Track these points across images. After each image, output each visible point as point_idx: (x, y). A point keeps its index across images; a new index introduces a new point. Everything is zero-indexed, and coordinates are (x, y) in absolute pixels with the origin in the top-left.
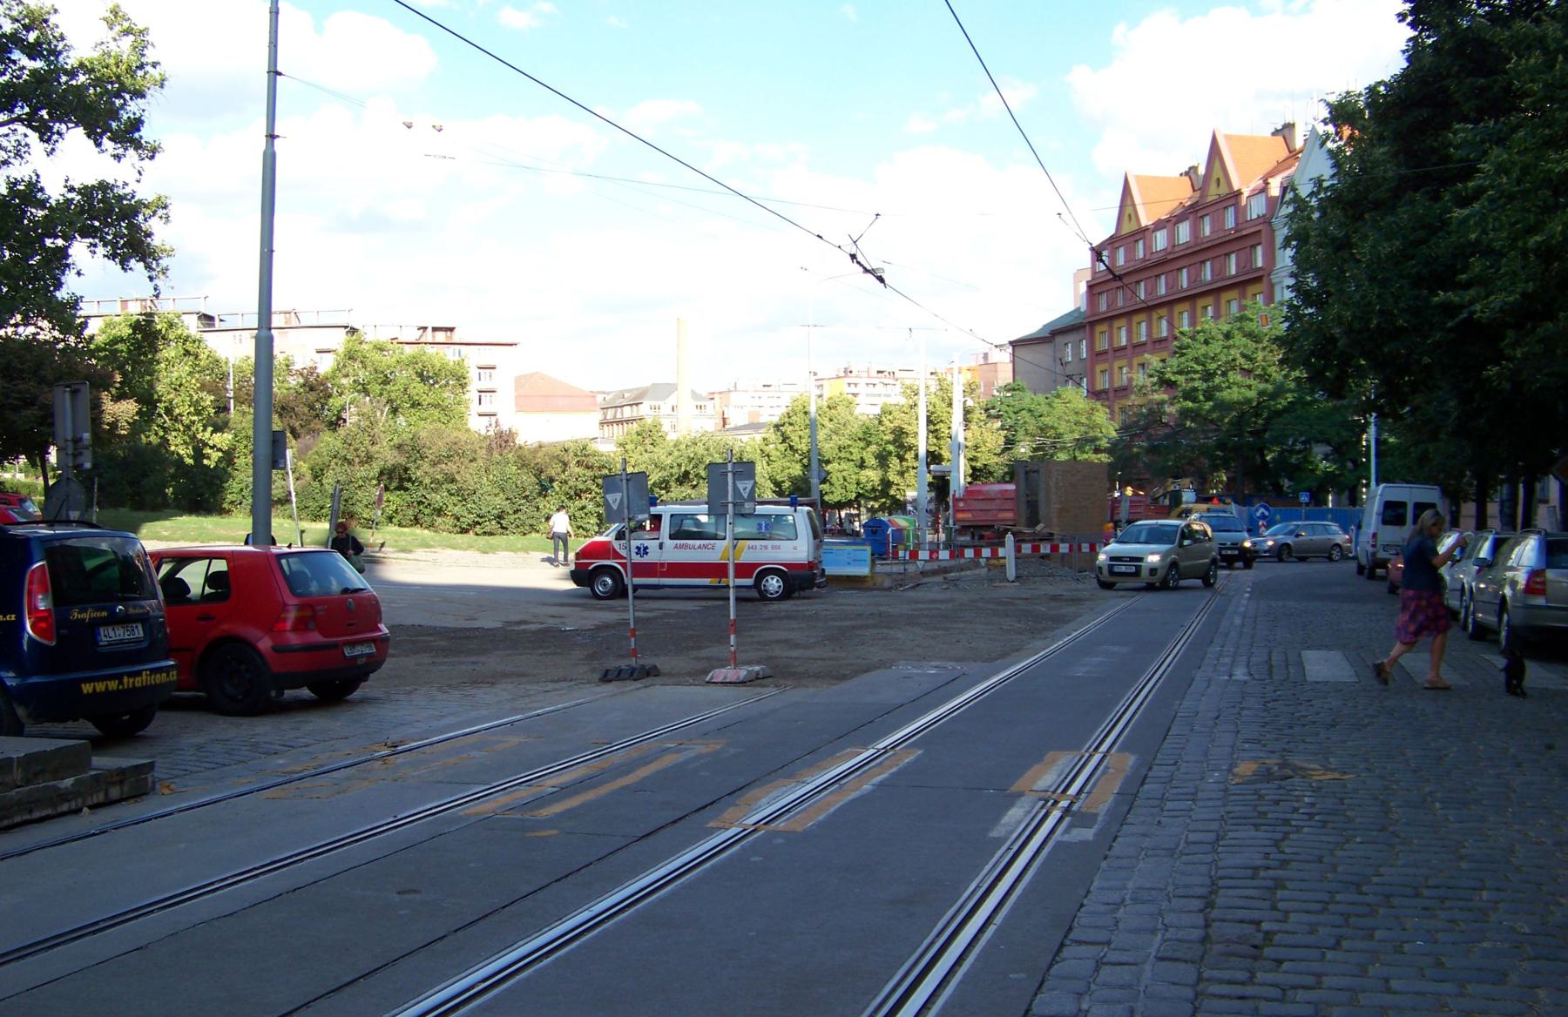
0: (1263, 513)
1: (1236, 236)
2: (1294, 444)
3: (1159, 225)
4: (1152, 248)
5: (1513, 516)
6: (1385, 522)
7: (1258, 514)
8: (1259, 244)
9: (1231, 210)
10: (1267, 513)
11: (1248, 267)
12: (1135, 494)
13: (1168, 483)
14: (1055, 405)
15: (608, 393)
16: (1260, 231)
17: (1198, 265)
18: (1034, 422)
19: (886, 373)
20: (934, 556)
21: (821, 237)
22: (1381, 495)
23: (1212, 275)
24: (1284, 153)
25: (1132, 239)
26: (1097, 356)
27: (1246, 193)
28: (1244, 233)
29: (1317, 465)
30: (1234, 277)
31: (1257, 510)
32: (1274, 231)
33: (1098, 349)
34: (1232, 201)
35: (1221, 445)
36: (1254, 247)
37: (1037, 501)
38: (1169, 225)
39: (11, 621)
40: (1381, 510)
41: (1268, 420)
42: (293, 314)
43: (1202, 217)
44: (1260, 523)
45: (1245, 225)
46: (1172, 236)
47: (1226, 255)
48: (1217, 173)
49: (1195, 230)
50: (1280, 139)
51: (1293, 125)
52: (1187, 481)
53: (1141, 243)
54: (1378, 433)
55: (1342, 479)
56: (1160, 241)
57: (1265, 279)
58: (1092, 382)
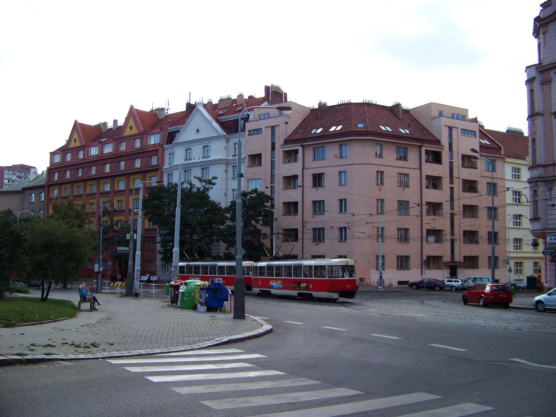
5: (344, 271)
11: (148, 165)
17: (89, 168)
23: (110, 170)
28: (148, 150)
30: (57, 181)
32: (164, 150)
39: (3, 179)
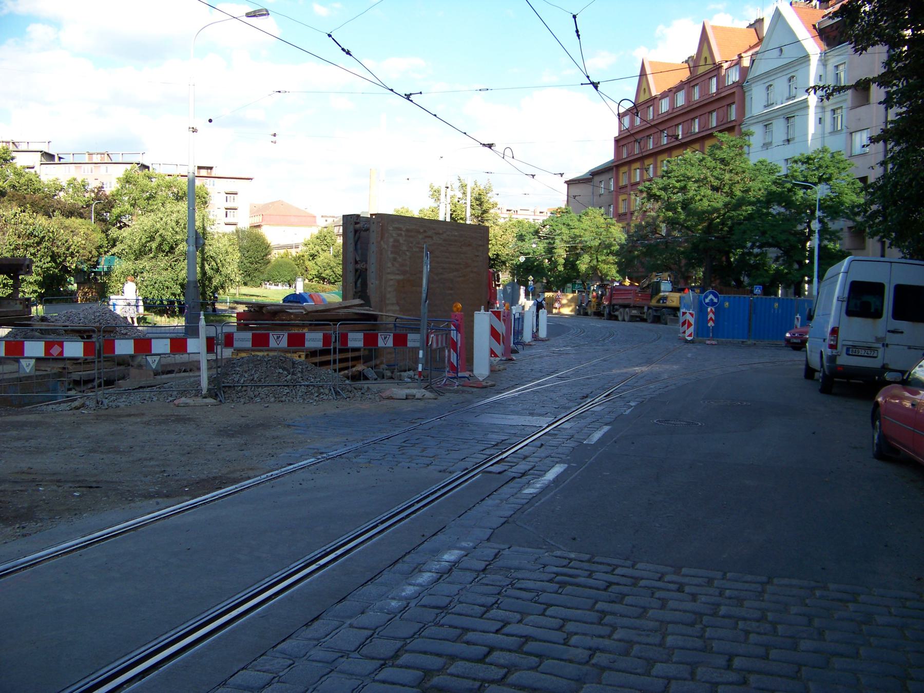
0: (712, 300)
1: (717, 97)
2: (752, 247)
3: (664, 95)
4: (658, 111)
6: (849, 313)
7: (707, 300)
8: (733, 103)
9: (714, 80)
10: (715, 300)
12: (631, 284)
13: (652, 276)
14: (583, 221)
15: (336, 218)
16: (734, 93)
18: (567, 232)
19: (512, 211)
20: (55, 351)
21: (348, 53)
22: (846, 272)
24: (756, 40)
25: (645, 106)
26: (620, 189)
27: (725, 66)
28: (723, 95)
29: (770, 266)
31: (706, 297)
33: (621, 185)
34: (715, 73)
35: (695, 247)
36: (729, 105)
37: (366, 269)
38: (671, 94)
40: (846, 295)
41: (731, 228)
42: (106, 155)
43: (693, 86)
44: (709, 309)
45: (723, 90)
46: (673, 102)
47: (709, 112)
48: (705, 53)
49: (688, 97)
50: (753, 30)
51: (763, 19)
52: (666, 274)
53: (651, 108)
54: (821, 240)
55: (789, 276)
56: (665, 106)
57: (737, 128)
58: (616, 208)
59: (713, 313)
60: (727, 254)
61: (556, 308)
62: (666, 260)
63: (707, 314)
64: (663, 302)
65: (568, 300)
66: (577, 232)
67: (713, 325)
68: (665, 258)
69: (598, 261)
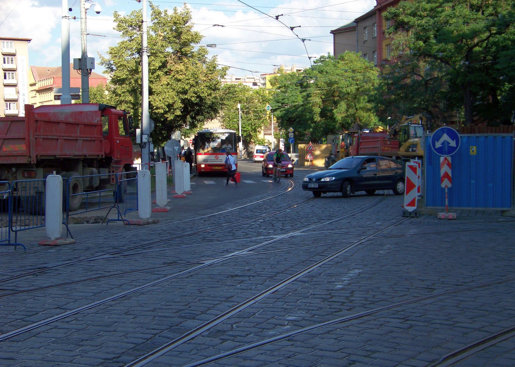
7: (438, 145)
10: (453, 144)
13: (403, 120)
31: (437, 138)
44: (442, 159)
59: (448, 164)
60: (493, 91)
61: (308, 161)
62: (424, 102)
63: (439, 167)
64: (413, 151)
65: (321, 151)
66: (334, 78)
67: (450, 185)
68: (423, 100)
69: (357, 109)
